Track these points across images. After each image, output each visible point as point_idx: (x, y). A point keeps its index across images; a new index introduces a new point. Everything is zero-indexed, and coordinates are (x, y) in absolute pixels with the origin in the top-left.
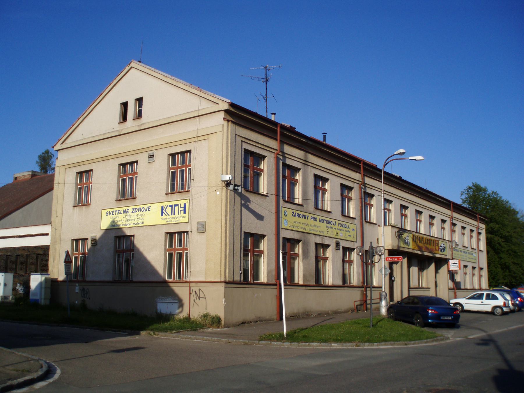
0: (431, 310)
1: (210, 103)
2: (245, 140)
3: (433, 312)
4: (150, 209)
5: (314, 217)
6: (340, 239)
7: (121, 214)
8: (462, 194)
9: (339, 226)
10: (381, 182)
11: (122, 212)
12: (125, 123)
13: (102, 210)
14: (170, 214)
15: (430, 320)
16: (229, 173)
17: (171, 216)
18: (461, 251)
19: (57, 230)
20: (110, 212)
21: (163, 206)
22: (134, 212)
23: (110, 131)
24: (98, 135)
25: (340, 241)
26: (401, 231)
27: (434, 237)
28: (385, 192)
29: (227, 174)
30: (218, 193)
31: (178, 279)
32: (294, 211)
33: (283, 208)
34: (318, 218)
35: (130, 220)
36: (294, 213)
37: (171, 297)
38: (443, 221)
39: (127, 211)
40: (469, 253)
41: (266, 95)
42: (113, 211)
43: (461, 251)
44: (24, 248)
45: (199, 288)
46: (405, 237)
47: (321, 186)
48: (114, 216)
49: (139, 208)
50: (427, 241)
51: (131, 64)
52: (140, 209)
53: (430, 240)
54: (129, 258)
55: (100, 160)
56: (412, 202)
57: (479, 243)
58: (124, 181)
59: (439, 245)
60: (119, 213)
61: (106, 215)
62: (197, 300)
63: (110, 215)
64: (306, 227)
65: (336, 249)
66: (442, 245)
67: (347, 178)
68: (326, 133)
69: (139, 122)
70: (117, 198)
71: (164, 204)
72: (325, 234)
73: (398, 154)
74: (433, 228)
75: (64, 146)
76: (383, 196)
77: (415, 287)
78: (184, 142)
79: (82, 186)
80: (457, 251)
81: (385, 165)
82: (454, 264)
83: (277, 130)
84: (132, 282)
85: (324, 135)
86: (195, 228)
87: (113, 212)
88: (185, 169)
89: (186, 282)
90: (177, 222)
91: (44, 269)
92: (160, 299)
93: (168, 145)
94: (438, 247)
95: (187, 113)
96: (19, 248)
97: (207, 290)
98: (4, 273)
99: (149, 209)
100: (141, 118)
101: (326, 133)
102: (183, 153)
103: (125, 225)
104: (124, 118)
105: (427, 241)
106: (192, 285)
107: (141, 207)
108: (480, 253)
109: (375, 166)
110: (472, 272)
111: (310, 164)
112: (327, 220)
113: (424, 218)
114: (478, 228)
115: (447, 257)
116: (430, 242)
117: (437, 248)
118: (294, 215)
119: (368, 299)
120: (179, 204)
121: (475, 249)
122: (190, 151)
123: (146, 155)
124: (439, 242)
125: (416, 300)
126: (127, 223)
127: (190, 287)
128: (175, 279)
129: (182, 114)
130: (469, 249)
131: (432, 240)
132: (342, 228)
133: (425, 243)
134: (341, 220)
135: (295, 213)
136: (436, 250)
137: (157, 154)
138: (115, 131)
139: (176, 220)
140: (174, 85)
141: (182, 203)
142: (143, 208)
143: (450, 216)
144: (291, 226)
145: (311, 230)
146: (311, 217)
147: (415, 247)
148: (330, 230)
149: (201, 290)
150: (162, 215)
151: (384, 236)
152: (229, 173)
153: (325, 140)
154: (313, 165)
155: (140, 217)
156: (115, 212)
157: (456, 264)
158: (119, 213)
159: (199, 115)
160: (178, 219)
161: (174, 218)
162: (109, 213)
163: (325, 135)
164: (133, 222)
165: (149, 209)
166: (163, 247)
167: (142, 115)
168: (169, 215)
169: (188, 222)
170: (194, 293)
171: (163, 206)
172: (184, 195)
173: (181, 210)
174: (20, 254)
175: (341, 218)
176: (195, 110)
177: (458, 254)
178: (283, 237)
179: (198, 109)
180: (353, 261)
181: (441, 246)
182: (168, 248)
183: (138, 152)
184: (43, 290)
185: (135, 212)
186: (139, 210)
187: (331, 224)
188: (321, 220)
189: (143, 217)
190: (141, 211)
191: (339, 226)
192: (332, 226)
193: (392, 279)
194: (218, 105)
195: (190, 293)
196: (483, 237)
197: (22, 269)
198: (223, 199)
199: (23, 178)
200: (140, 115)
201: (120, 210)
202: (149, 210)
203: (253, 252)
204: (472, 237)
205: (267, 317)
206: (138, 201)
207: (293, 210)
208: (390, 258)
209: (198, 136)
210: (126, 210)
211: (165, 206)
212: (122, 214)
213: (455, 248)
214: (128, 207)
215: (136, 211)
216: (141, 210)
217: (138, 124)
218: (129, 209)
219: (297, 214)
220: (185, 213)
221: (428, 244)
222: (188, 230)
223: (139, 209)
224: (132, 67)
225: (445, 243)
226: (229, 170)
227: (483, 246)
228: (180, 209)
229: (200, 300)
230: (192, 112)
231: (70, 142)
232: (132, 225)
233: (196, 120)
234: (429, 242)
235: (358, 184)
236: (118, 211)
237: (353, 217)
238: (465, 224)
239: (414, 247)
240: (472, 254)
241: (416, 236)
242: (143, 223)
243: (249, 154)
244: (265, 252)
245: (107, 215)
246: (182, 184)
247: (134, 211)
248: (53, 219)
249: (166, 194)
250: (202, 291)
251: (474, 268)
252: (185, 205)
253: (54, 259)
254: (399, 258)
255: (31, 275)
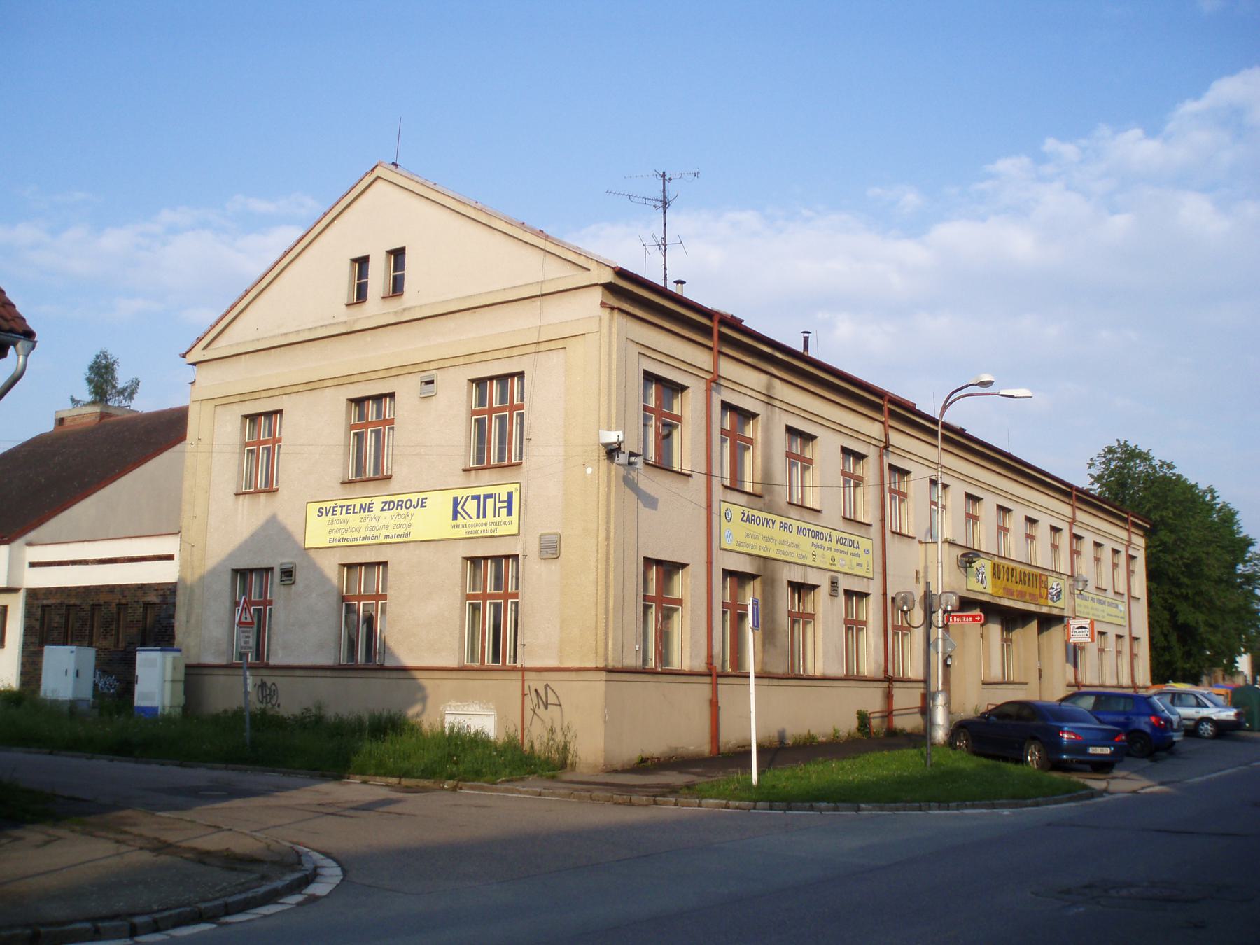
0: (1068, 732)
1: (569, 266)
2: (647, 351)
3: (1073, 737)
4: (425, 503)
5: (786, 524)
6: (841, 572)
7: (354, 513)
8: (1091, 466)
9: (837, 543)
10: (937, 447)
11: (357, 509)
12: (363, 304)
13: (307, 503)
14: (474, 515)
15: (1065, 755)
16: (614, 426)
17: (475, 521)
18: (1093, 599)
19: (195, 549)
20: (326, 508)
21: (457, 498)
22: (385, 510)
23: (327, 323)
24: (297, 332)
25: (840, 577)
26: (969, 557)
27: (1036, 567)
28: (944, 470)
29: (609, 429)
30: (589, 470)
31: (493, 663)
32: (746, 510)
33: (722, 503)
34: (796, 524)
35: (377, 528)
36: (746, 515)
37: (477, 702)
38: (1055, 530)
39: (369, 508)
40: (1110, 604)
41: (664, 239)
42: (334, 507)
43: (1093, 599)
44: (111, 589)
45: (545, 683)
46: (977, 568)
47: (799, 454)
48: (338, 517)
49: (399, 501)
50: (1022, 576)
51: (376, 170)
52: (400, 503)
53: (1029, 574)
54: (374, 614)
55: (301, 388)
56: (990, 488)
57: (1132, 579)
58: (360, 438)
59: (1047, 584)
60: (349, 512)
61: (318, 516)
62: (541, 711)
63: (327, 514)
64: (769, 545)
65: (831, 596)
66: (1055, 586)
67: (855, 434)
68: (809, 333)
69: (395, 305)
70: (344, 475)
71: (460, 494)
72: (809, 562)
73: (976, 385)
74: (902, 506)
75: (210, 354)
76: (941, 478)
77: (996, 680)
78: (506, 353)
79: (255, 447)
80: (1085, 599)
81: (945, 408)
82: (1080, 630)
83: (937, 432)
84: (382, 668)
85: (805, 337)
86: (533, 547)
87: (335, 509)
88: (507, 413)
89: (514, 669)
90: (490, 534)
91: (162, 636)
92: (450, 707)
93: (467, 360)
94: (1046, 590)
95: (515, 287)
96: (99, 589)
97: (564, 688)
98: (75, 647)
99: (422, 503)
100: (402, 295)
101: (809, 333)
102: (503, 379)
103: (364, 539)
104: (361, 294)
105: (1022, 576)
106: (528, 675)
107: (405, 497)
108: (1133, 603)
109: (911, 405)
110: (1115, 647)
111: (874, 442)
112: (813, 531)
113: (1016, 522)
114: (1129, 544)
115: (1066, 613)
116: (1029, 579)
117: (1044, 592)
118: (745, 519)
119: (894, 708)
120: (495, 494)
121: (1123, 594)
122: (521, 375)
123: (415, 381)
124: (1047, 578)
125: (1025, 713)
126: (369, 534)
127: (523, 681)
128: (486, 663)
129: (501, 290)
130: (1110, 593)
131: (1033, 575)
132: (843, 548)
133: (1018, 580)
134: (842, 530)
135: (748, 515)
136: (1041, 597)
137: (440, 377)
138: (338, 324)
139: (489, 530)
140: (481, 223)
141: (503, 491)
142: (407, 501)
143: (1070, 518)
144: (740, 544)
145: (779, 552)
146: (781, 523)
147: (998, 591)
148: (819, 551)
149: (550, 688)
150: (455, 518)
151: (942, 566)
152: (614, 426)
153: (806, 347)
154: (785, 407)
155: (402, 521)
156: (339, 509)
157: (1083, 630)
158: (349, 512)
159: (543, 293)
160: (493, 527)
161: (485, 525)
162: (324, 511)
163: (808, 337)
164: (384, 533)
165: (422, 503)
166: (458, 590)
167: (405, 289)
168: (471, 518)
169: (519, 535)
170: (534, 694)
171: (457, 498)
172: (508, 475)
173: (500, 508)
174: (102, 602)
175: (841, 524)
176: (534, 281)
177: (1086, 607)
178: (644, 558)
179: (540, 280)
180: (866, 622)
181: (1052, 588)
182: (468, 592)
183: (394, 372)
184: (168, 686)
185: (389, 509)
186: (398, 505)
187: (822, 540)
188: (800, 531)
189: (408, 521)
190: (404, 507)
191: (837, 543)
192: (824, 543)
193: (64, 640)
194: (589, 272)
195: (524, 695)
196: (1140, 567)
197: (106, 638)
198: (600, 483)
199: (78, 422)
200: (397, 287)
201: (351, 505)
202: (422, 507)
203: (659, 599)
204: (1115, 566)
205: (692, 748)
206: (394, 485)
207: (744, 508)
208: (955, 617)
209: (540, 340)
210: (366, 504)
211: (463, 497)
212: (357, 513)
213: (1082, 592)
214: (371, 499)
215: (391, 507)
216: (404, 505)
217: (395, 310)
218: (373, 503)
219: (752, 516)
220: (510, 513)
221: (1025, 584)
222: (517, 553)
223: (398, 503)
224: (378, 178)
225: (1059, 581)
226: (614, 420)
227: (1140, 586)
228: (498, 505)
229: (549, 709)
230: (526, 285)
231: (226, 346)
232: (382, 540)
233: (534, 304)
234: (1027, 579)
235: (877, 448)
236: (348, 506)
237: (866, 522)
238: (1101, 537)
239: (996, 590)
240: (1117, 606)
241: (999, 566)
242: (408, 535)
243: (652, 382)
244: (688, 604)
245: (320, 514)
246: (499, 448)
247: (387, 507)
248: (185, 522)
249: (465, 470)
250: (552, 690)
251: (1119, 637)
252: (510, 495)
253: (189, 615)
254: (976, 616)
255: (138, 652)
